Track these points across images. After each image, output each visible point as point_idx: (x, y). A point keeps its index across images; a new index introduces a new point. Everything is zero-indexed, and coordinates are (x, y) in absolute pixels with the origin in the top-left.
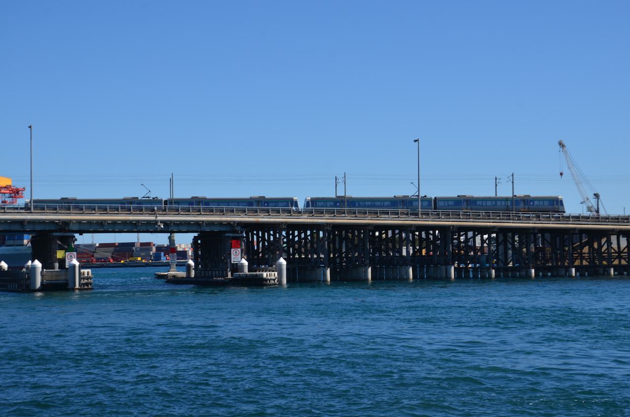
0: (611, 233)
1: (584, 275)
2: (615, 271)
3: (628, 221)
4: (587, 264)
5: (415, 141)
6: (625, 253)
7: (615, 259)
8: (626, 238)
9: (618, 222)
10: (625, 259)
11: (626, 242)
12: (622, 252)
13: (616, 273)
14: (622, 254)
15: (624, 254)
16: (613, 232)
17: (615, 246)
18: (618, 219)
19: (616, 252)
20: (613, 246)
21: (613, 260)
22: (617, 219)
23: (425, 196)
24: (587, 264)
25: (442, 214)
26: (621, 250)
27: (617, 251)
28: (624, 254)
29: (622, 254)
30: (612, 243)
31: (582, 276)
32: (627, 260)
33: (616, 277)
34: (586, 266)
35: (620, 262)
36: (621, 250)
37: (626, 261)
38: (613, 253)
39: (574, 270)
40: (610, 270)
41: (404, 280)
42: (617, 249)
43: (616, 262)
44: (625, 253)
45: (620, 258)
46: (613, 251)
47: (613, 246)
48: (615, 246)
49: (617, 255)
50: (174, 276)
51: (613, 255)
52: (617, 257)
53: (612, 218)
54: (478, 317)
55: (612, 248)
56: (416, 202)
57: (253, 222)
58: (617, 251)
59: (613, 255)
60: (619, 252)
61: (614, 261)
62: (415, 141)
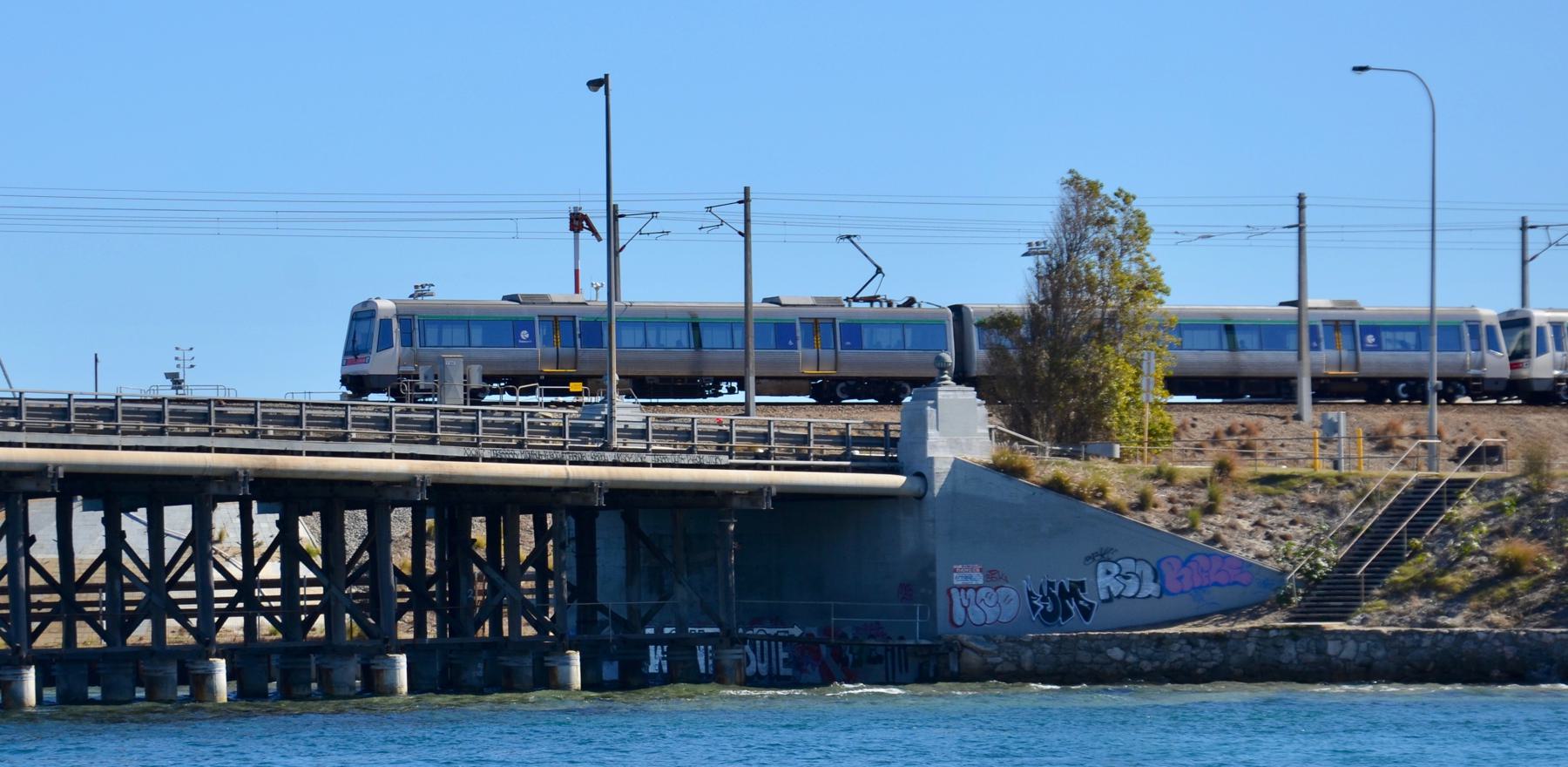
0: (29, 485)
1: (263, 695)
2: (41, 684)
3: (112, 425)
4: (189, 639)
5: (595, 84)
6: (95, 588)
7: (45, 621)
8: (101, 514)
9: (67, 430)
10: (92, 620)
11: (102, 530)
12: (82, 586)
13: (50, 693)
14: (81, 597)
15: (93, 597)
16: (33, 480)
17: (45, 551)
18: (64, 413)
19: (51, 587)
20: (36, 552)
21: (35, 625)
22: (59, 417)
23: (910, 302)
24: (189, 639)
25: (172, 412)
26: (78, 576)
27: (58, 579)
28: (93, 597)
29: (81, 597)
30: (32, 540)
31: (72, 697)
32: (193, 622)
33: (46, 711)
34: (90, 654)
35: (70, 635)
36: (78, 576)
37: (98, 629)
38: (220, 585)
39: (30, 677)
40: (19, 678)
41: (308, 697)
42: (55, 571)
43: (51, 637)
44: (95, 588)
45: (69, 613)
46: (36, 579)
47: (36, 552)
48: (45, 551)
49: (56, 598)
50: (229, 678)
51: (35, 598)
52: (56, 613)
53: (35, 412)
54: (1362, 748)
55: (31, 562)
56: (708, 338)
57: (129, 467)
58: (58, 579)
59: (35, 598)
60: (69, 583)
61: (40, 630)
62: (595, 84)
